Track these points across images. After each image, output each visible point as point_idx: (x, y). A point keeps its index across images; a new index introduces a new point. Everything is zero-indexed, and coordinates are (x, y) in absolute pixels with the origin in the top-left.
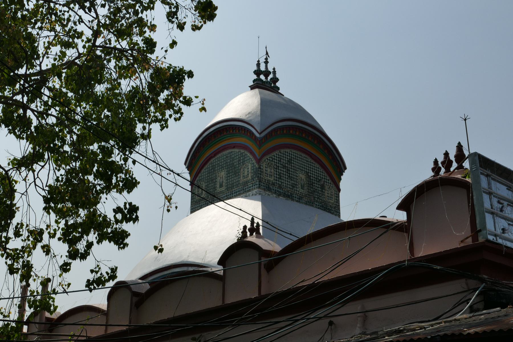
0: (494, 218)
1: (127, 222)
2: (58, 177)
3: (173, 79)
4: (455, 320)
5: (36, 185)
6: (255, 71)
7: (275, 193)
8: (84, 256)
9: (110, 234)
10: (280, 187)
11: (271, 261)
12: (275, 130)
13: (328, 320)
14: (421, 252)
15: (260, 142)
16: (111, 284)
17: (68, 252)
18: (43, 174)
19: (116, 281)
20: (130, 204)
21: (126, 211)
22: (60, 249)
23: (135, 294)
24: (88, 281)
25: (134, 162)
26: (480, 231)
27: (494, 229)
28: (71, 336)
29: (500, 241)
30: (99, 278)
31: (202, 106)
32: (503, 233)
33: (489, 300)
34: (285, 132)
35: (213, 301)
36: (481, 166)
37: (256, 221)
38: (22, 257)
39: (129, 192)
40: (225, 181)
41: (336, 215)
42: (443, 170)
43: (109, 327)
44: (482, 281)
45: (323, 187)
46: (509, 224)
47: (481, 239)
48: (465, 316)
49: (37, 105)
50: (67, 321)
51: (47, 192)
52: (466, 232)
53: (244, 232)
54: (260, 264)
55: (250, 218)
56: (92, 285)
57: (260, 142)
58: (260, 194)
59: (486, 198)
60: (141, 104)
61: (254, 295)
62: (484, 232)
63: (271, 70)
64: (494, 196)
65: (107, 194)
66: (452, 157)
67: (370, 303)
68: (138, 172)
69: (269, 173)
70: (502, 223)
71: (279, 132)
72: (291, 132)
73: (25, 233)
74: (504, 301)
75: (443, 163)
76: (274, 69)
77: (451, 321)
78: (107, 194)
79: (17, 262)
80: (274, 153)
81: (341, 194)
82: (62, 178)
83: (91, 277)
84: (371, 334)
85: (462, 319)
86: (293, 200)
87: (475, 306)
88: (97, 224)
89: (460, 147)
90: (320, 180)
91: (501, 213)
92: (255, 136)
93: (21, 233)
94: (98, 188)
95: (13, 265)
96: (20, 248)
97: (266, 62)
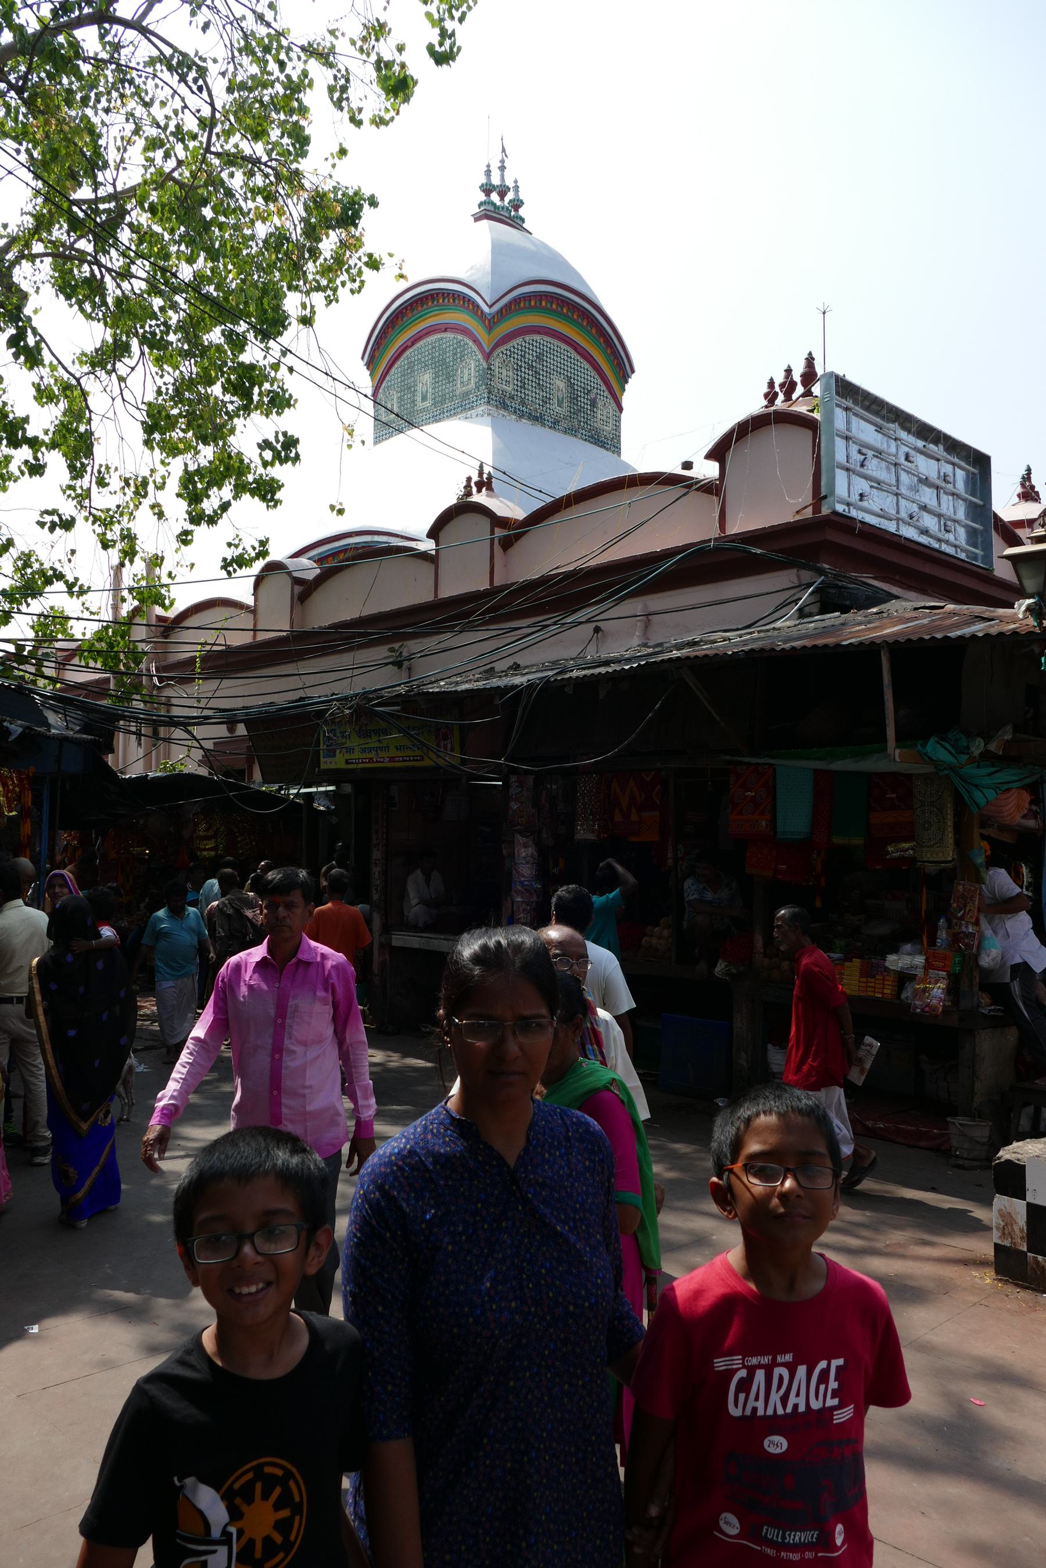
0: (849, 477)
1: (281, 464)
2: (160, 388)
3: (345, 211)
4: (774, 629)
5: (124, 400)
6: (482, 185)
7: (515, 412)
8: (212, 520)
9: (251, 484)
10: (523, 403)
11: (510, 534)
12: (516, 301)
13: (594, 625)
14: (735, 527)
15: (490, 323)
16: (259, 565)
17: (188, 512)
18: (135, 381)
19: (268, 559)
20: (285, 434)
21: (279, 447)
22: (177, 509)
23: (297, 581)
24: (225, 560)
25: (291, 370)
26: (825, 497)
27: (846, 494)
28: (201, 644)
29: (854, 513)
30: (241, 555)
31: (399, 271)
32: (861, 500)
33: (830, 600)
34: (533, 303)
35: (422, 595)
36: (837, 393)
37: (487, 469)
38: (119, 522)
39: (279, 414)
40: (430, 390)
41: (613, 452)
42: (781, 397)
43: (258, 633)
44: (821, 572)
45: (593, 403)
46: (871, 487)
47: (825, 511)
48: (788, 623)
49: (114, 260)
50: (188, 623)
51: (145, 413)
52: (806, 497)
53: (468, 486)
54: (492, 540)
55: (477, 465)
56: (232, 565)
57: (490, 323)
58: (489, 414)
59: (840, 444)
60: (289, 257)
61: (484, 586)
62: (830, 499)
63: (511, 185)
64: (854, 442)
65: (245, 419)
66: (797, 377)
67: (657, 602)
68: (293, 385)
69: (506, 379)
70: (861, 485)
71: (522, 305)
72: (544, 303)
73: (115, 483)
74: (848, 603)
75: (782, 386)
76: (516, 182)
77: (768, 631)
78: (245, 419)
79: (111, 530)
80: (514, 343)
81: (623, 416)
82: (167, 389)
83: (230, 553)
84: (654, 647)
85: (783, 627)
86: (543, 425)
87: (807, 609)
88: (229, 469)
89: (810, 361)
90: (589, 391)
91: (861, 470)
92: (482, 311)
93: (107, 481)
94: (230, 407)
95: (104, 534)
96: (114, 508)
97: (502, 168)
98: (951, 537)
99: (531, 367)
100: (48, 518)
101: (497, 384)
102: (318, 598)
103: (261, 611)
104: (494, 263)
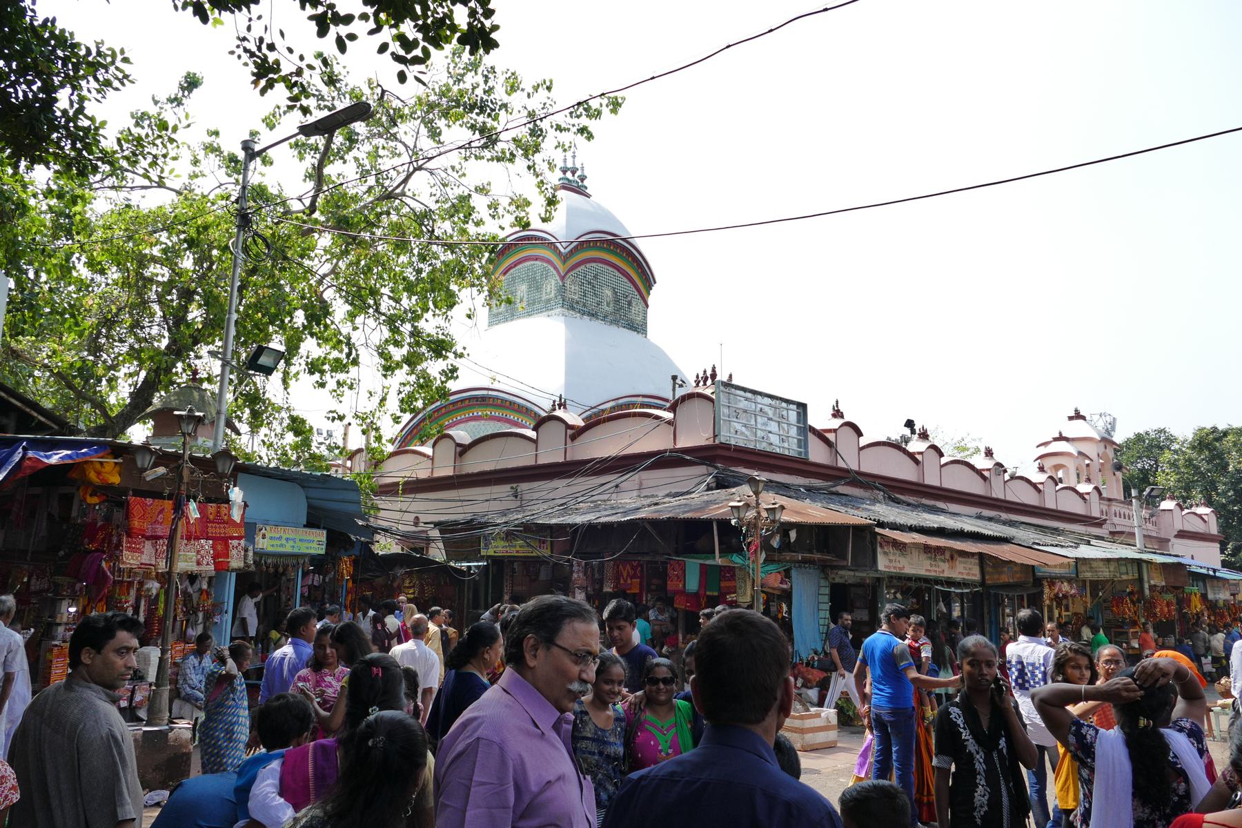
10: (584, 305)
14: (679, 445)
23: (458, 445)
44: (716, 468)
45: (630, 303)
47: (717, 442)
57: (565, 258)
59: (726, 411)
98: (786, 445)
99: (590, 283)
100: (331, 415)
101: (568, 295)
102: (470, 455)
103: (436, 460)
104: (568, 221)
